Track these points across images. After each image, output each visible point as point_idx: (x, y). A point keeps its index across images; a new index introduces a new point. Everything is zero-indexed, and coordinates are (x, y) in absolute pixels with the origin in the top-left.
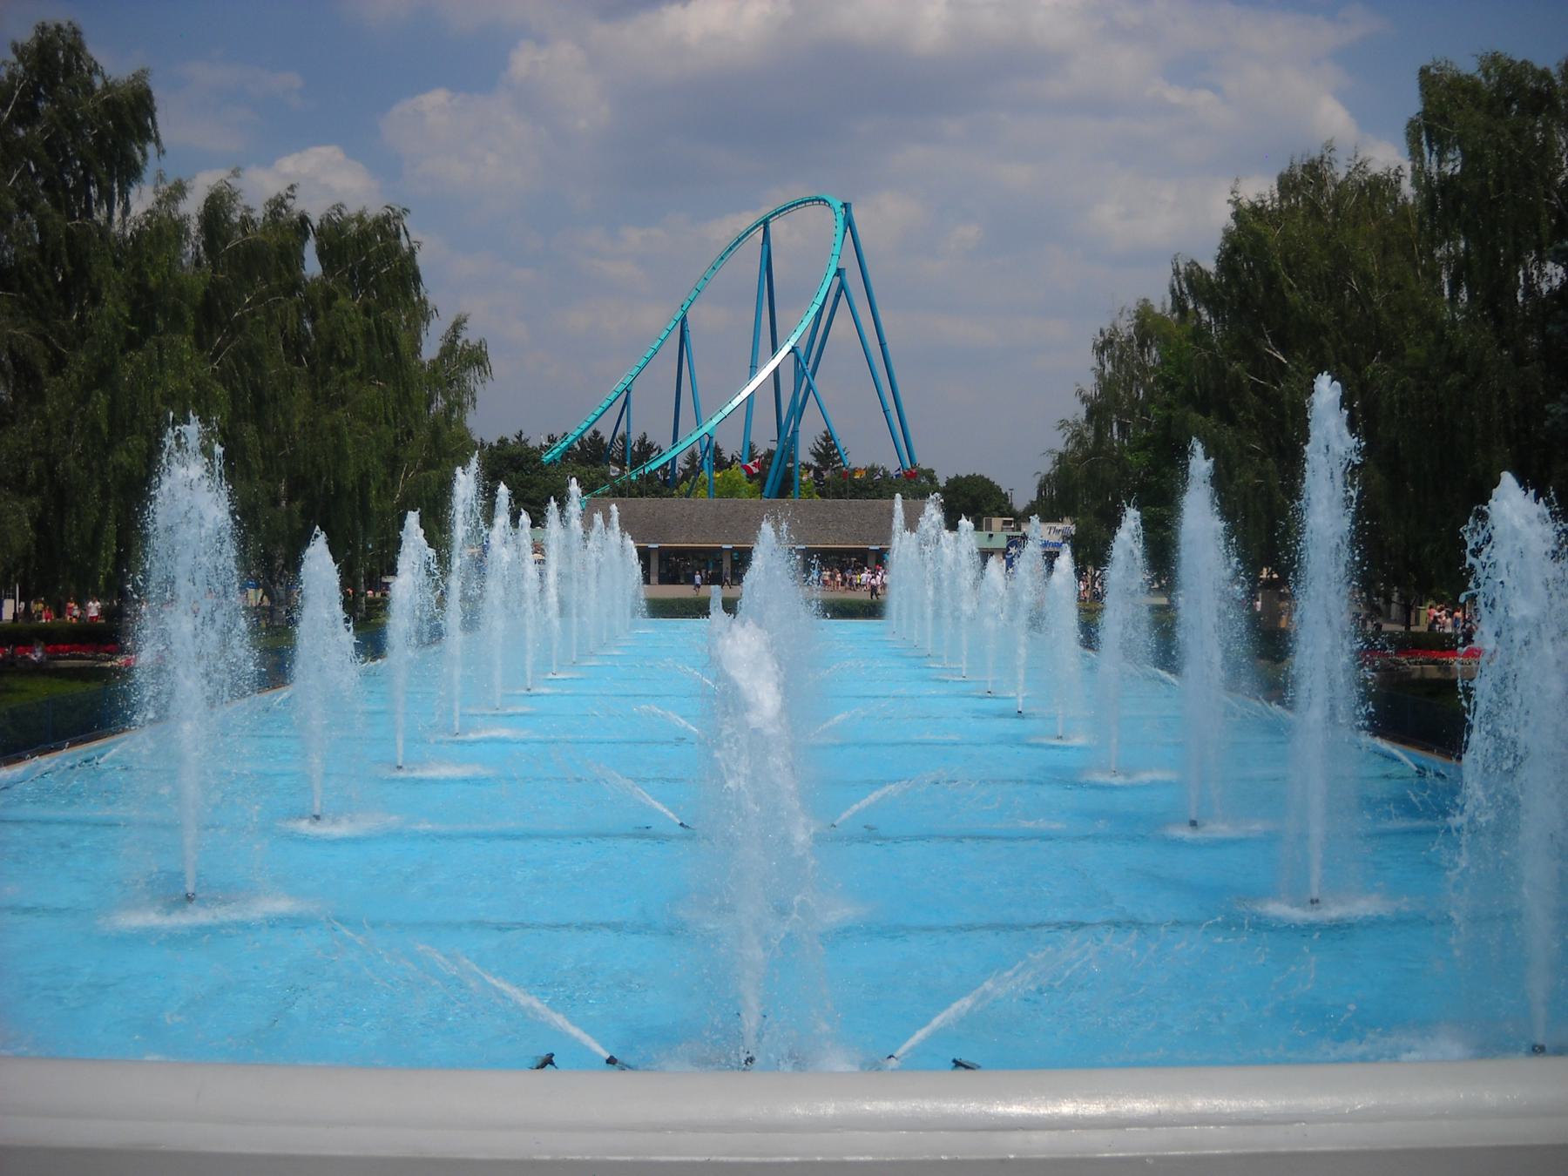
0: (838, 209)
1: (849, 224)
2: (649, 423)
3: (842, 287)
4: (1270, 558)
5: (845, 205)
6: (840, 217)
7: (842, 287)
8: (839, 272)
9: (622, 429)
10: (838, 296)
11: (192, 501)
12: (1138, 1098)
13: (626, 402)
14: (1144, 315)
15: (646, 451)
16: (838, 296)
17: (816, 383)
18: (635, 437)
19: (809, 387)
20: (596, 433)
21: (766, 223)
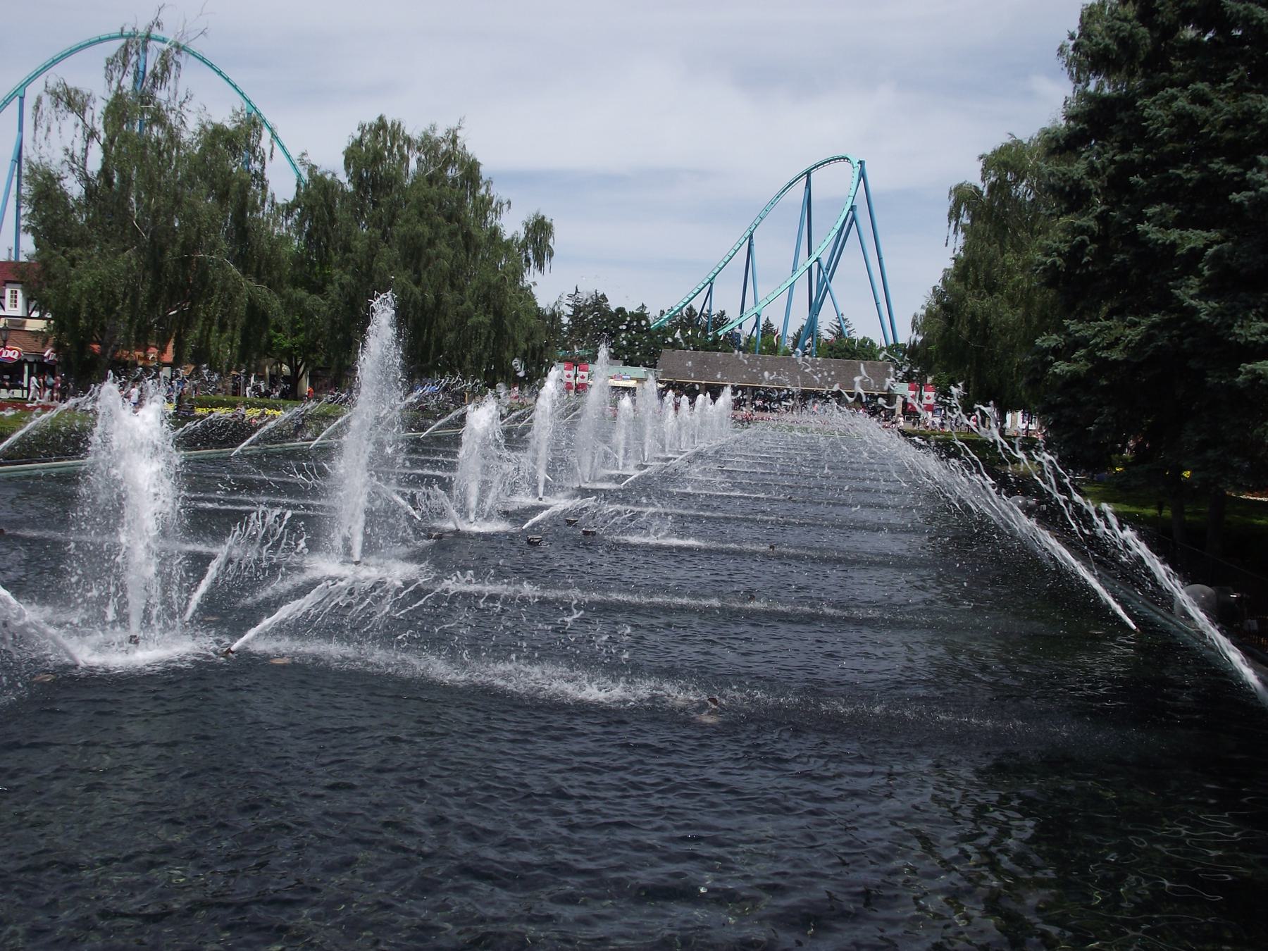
0: (856, 164)
1: (862, 175)
2: (725, 301)
3: (854, 218)
4: (648, 894)
5: (861, 162)
6: (857, 170)
7: (854, 218)
8: (852, 208)
9: (707, 306)
10: (851, 225)
11: (381, 339)
12: (1250, 666)
13: (710, 291)
14: (641, 316)
15: (721, 320)
16: (851, 225)
17: (832, 285)
18: (715, 312)
19: (827, 288)
20: (691, 309)
21: (808, 173)
